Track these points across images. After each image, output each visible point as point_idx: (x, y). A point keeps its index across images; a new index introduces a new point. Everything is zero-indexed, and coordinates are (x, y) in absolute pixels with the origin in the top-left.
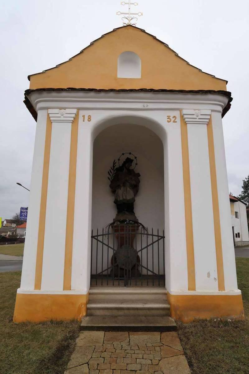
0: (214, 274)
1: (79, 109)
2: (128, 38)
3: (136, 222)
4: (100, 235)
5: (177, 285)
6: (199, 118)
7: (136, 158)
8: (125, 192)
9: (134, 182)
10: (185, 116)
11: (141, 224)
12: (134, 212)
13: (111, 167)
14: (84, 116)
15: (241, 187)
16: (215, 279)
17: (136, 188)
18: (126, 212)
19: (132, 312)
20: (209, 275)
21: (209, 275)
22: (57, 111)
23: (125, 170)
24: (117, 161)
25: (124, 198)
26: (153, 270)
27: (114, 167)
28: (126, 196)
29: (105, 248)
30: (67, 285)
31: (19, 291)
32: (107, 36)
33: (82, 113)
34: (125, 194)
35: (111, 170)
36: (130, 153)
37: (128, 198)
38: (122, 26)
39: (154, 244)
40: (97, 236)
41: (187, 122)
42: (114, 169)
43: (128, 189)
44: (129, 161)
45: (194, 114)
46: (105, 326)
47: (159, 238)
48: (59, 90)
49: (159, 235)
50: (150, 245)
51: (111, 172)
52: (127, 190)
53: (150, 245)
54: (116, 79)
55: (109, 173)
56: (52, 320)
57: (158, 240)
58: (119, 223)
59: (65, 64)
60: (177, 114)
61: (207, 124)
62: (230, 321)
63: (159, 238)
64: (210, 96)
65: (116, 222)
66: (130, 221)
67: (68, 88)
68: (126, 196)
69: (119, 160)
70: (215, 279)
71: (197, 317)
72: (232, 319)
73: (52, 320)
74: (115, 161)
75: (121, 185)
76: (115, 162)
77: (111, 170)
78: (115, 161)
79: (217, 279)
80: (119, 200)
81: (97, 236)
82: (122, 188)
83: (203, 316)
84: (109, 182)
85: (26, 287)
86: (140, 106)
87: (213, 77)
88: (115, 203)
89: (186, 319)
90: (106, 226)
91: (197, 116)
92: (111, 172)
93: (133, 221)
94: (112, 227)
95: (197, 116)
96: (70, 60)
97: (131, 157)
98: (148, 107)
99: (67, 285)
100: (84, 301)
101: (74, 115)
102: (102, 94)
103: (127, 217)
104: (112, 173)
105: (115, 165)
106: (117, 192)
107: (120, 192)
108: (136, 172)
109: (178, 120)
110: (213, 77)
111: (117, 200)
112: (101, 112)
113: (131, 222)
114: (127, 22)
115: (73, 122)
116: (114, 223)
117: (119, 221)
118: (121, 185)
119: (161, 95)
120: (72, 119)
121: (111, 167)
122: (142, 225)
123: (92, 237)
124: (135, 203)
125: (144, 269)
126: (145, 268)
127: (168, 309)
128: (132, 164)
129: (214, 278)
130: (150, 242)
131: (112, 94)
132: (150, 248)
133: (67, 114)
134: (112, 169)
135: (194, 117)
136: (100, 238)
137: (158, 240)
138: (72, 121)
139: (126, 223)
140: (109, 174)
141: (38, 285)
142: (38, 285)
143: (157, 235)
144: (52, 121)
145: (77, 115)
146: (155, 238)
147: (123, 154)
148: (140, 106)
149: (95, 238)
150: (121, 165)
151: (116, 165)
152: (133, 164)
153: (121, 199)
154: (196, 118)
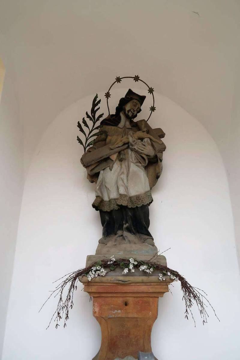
2: (88, 256)
3: (161, 268)
7: (151, 91)
8: (124, 177)
9: (148, 150)
11: (176, 274)
12: (149, 234)
13: (87, 113)
15: (77, 126)
17: (153, 164)
18: (126, 234)
23: (123, 121)
24: (101, 96)
25: (122, 191)
27: (93, 111)
28: (127, 188)
34: (124, 181)
35: (87, 120)
36: (137, 78)
37: (133, 192)
42: (94, 117)
43: (134, 168)
44: (132, 99)
51: (86, 125)
52: (129, 170)
55: (79, 126)
58: (103, 271)
65: (94, 269)
66: (140, 264)
68: (127, 188)
69: (108, 95)
74: (96, 97)
75: (114, 157)
76: (98, 99)
77: (87, 120)
78: (96, 97)
80: (106, 199)
82: (116, 166)
84: (80, 151)
88: (97, 210)
90: (64, 279)
92: (86, 125)
93: (150, 265)
94: (87, 284)
97: (139, 90)
103: (128, 248)
104: (87, 126)
105: (96, 108)
106: (101, 176)
107: (111, 176)
108: (154, 124)
111: (102, 201)
113: (143, 268)
116: (86, 271)
117: (105, 265)
118: (114, 157)
121: (87, 113)
122: (181, 279)
124: (151, 207)
128: (142, 108)
134: (88, 116)
139: (126, 271)
140: (82, 130)
147: (118, 80)
150: (113, 112)
151: (99, 108)
152: (146, 106)
153: (114, 195)
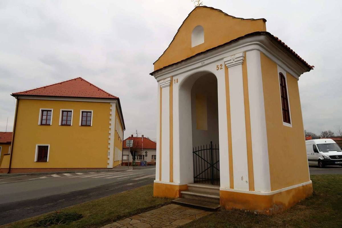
0: (246, 178)
1: (172, 77)
4: (197, 151)
5: (224, 185)
6: (235, 62)
16: (246, 182)
19: (202, 199)
20: (242, 178)
21: (242, 178)
29: (200, 159)
30: (171, 180)
31: (155, 181)
32: (185, 22)
33: (174, 78)
38: (195, 8)
40: (196, 152)
41: (228, 67)
45: (231, 60)
46: (187, 204)
54: (191, 49)
56: (166, 198)
59: (167, 50)
61: (242, 64)
62: (256, 213)
64: (241, 42)
67: (164, 67)
70: (246, 182)
71: (234, 207)
72: (257, 212)
73: (166, 198)
79: (248, 181)
81: (196, 152)
83: (239, 207)
85: (157, 180)
86: (200, 65)
87: (252, 20)
89: (228, 207)
91: (234, 60)
95: (165, 83)
96: (169, 46)
98: (205, 64)
99: (171, 180)
100: (178, 189)
101: (169, 82)
102: (179, 65)
110: (253, 20)
112: (181, 76)
114: (197, 4)
115: (170, 85)
119: (209, 54)
120: (169, 84)
123: (194, 152)
127: (218, 199)
129: (245, 181)
131: (183, 63)
133: (237, 59)
135: (232, 61)
136: (197, 153)
138: (241, 63)
141: (160, 179)
142: (160, 179)
145: (245, 57)
148: (200, 65)
149: (195, 153)
154: (233, 62)
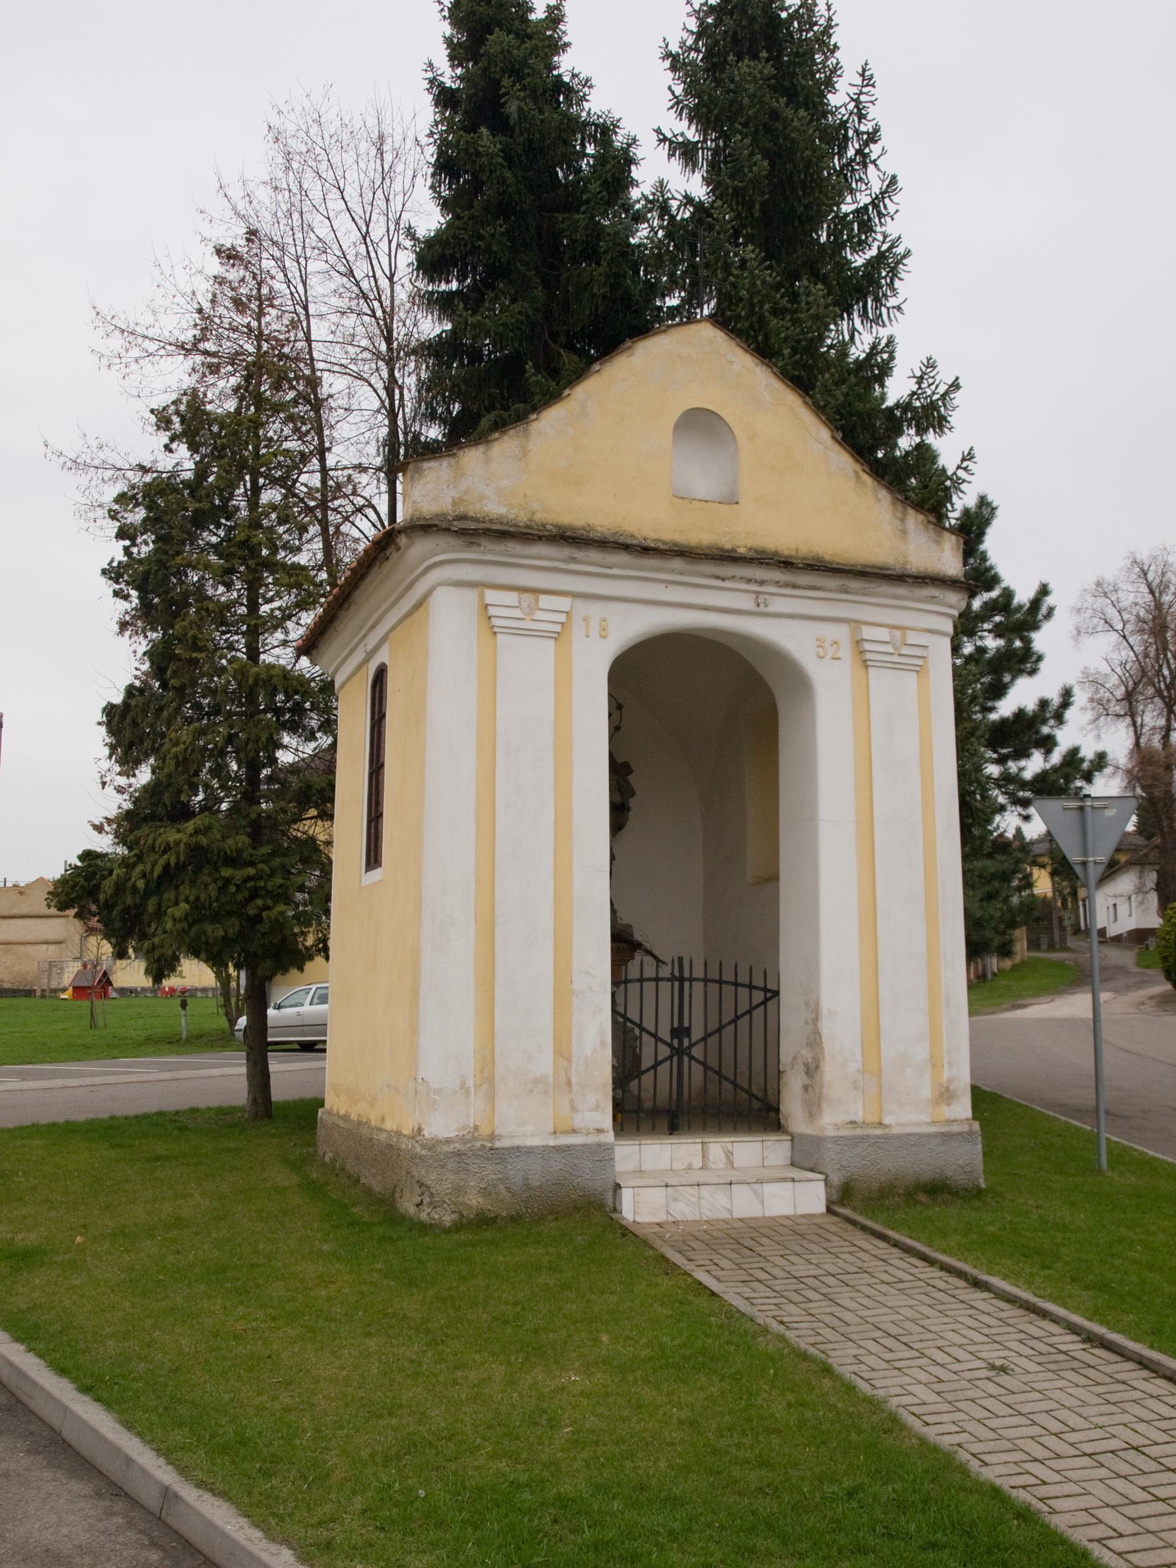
10: (867, 646)
14: (585, 619)
22: (511, 598)
26: (705, 1057)
39: (717, 1026)
47: (769, 995)
48: (528, 539)
49: (769, 987)
50: (757, 1006)
53: (757, 1006)
57: (764, 1003)
60: (841, 633)
63: (769, 995)
109: (846, 651)
125: (1120, 1502)
126: (709, 1068)
130: (743, 1007)
132: (743, 1023)
137: (764, 1003)
143: (754, 991)
144: (496, 630)
146: (759, 997)
